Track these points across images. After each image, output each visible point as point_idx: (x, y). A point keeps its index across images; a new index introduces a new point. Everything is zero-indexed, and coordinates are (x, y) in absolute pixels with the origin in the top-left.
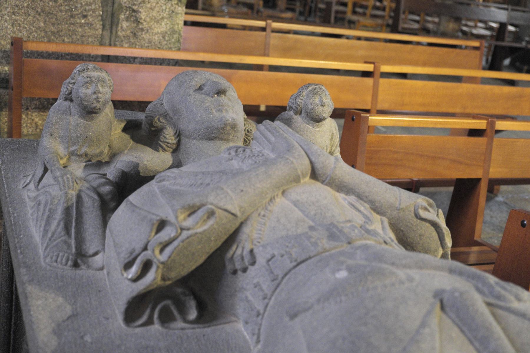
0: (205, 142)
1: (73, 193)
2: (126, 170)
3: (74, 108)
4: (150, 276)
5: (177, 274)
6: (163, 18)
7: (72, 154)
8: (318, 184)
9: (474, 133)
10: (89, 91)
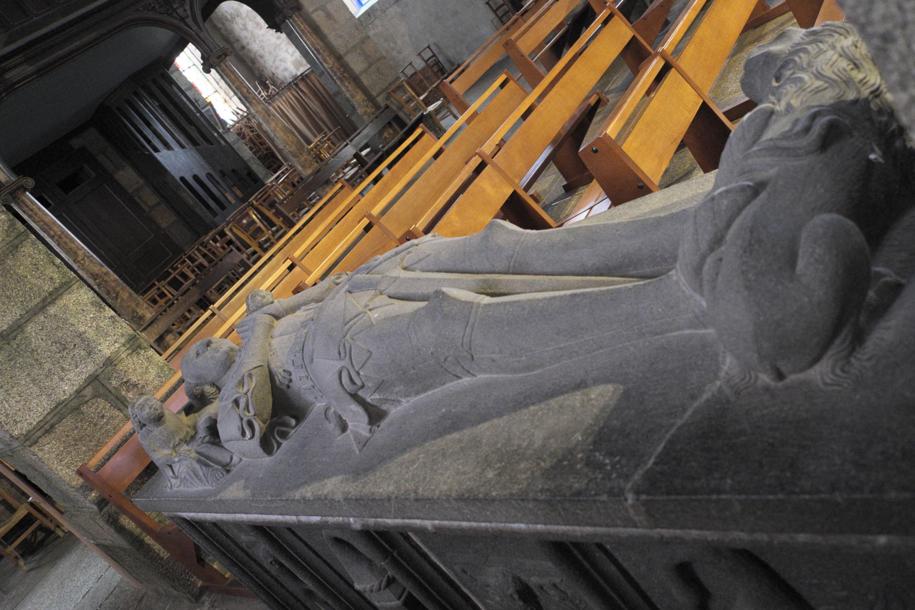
0: (228, 372)
1: (194, 455)
2: (208, 425)
3: (149, 427)
6: (147, 368)
7: (174, 448)
8: (283, 319)
9: (368, 228)
10: (147, 410)
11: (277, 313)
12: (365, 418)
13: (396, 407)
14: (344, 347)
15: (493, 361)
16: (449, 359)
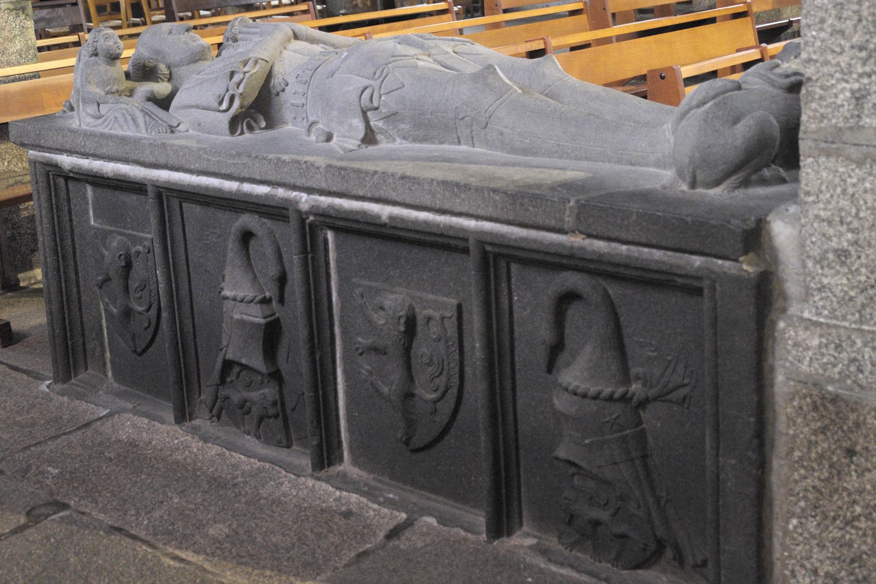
3: (100, 60)
4: (237, 103)
5: (250, 100)
11: (299, 34)
12: (361, 134)
13: (388, 142)
14: (383, 70)
15: (502, 134)
16: (467, 119)
